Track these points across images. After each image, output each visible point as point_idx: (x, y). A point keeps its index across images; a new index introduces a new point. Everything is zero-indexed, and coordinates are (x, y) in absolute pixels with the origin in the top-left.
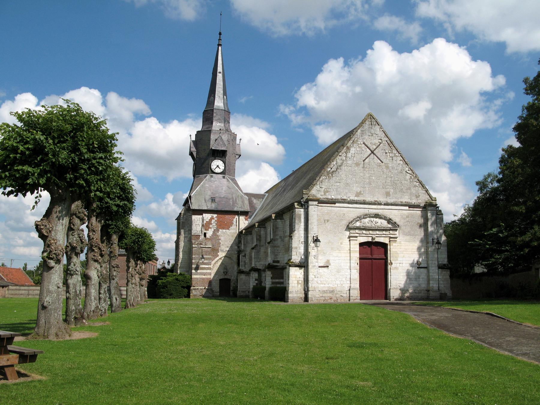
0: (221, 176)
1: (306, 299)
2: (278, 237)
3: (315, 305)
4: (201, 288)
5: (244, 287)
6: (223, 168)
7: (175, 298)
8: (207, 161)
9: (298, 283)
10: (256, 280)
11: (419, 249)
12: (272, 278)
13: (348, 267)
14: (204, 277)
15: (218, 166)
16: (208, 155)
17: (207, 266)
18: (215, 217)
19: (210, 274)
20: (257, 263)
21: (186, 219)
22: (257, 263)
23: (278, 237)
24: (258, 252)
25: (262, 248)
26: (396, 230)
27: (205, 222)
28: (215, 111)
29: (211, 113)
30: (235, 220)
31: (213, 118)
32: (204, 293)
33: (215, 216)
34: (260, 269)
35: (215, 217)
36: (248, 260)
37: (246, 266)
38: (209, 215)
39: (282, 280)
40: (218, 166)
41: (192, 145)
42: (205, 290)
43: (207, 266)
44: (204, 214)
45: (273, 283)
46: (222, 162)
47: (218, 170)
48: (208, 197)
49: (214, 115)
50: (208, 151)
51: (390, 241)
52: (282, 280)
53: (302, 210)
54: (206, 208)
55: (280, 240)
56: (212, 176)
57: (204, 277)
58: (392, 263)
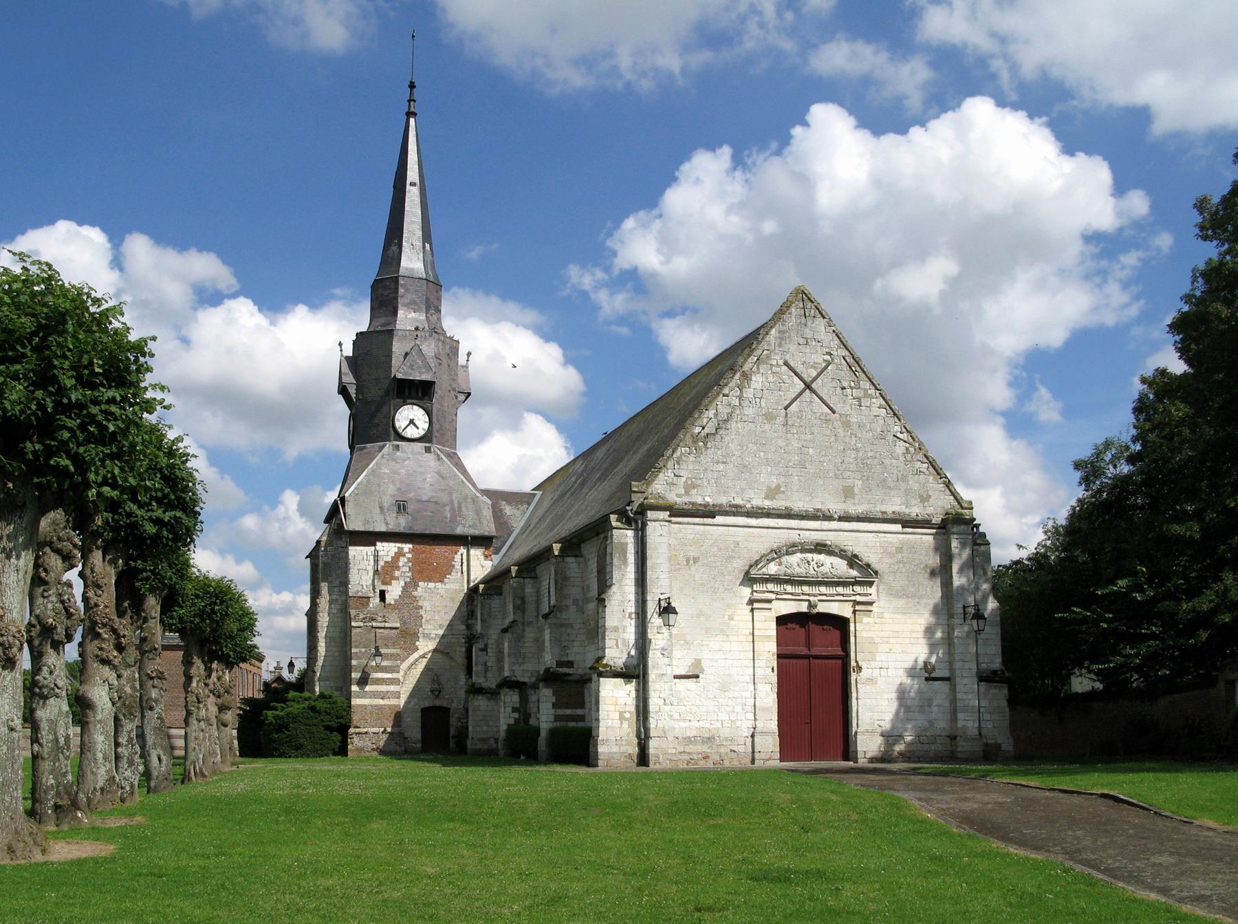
0: (420, 446)
1: (643, 758)
2: (569, 602)
3: (665, 774)
4: (376, 730)
5: (485, 728)
6: (426, 426)
7: (308, 756)
8: (384, 410)
9: (622, 718)
10: (514, 710)
11: (929, 631)
12: (554, 706)
13: (749, 679)
14: (381, 702)
15: (412, 422)
16: (387, 393)
17: (389, 676)
18: (406, 550)
19: (397, 695)
20: (516, 668)
21: (333, 556)
22: (516, 668)
23: (569, 602)
24: (519, 639)
25: (528, 630)
26: (871, 584)
27: (381, 563)
28: (401, 282)
29: (393, 286)
30: (458, 558)
31: (396, 298)
32: (382, 744)
33: (407, 547)
34: (524, 684)
35: (406, 550)
36: (493, 659)
37: (489, 675)
38: (392, 545)
39: (579, 712)
40: (412, 422)
41: (346, 369)
42: (385, 737)
43: (389, 676)
44: (378, 544)
45: (558, 718)
46: (421, 412)
47: (411, 432)
48: (388, 501)
49: (401, 291)
50: (385, 384)
51: (854, 612)
52: (579, 712)
53: (630, 533)
54: (383, 529)
55: (573, 609)
56: (397, 447)
57: (381, 702)
58: (859, 668)
